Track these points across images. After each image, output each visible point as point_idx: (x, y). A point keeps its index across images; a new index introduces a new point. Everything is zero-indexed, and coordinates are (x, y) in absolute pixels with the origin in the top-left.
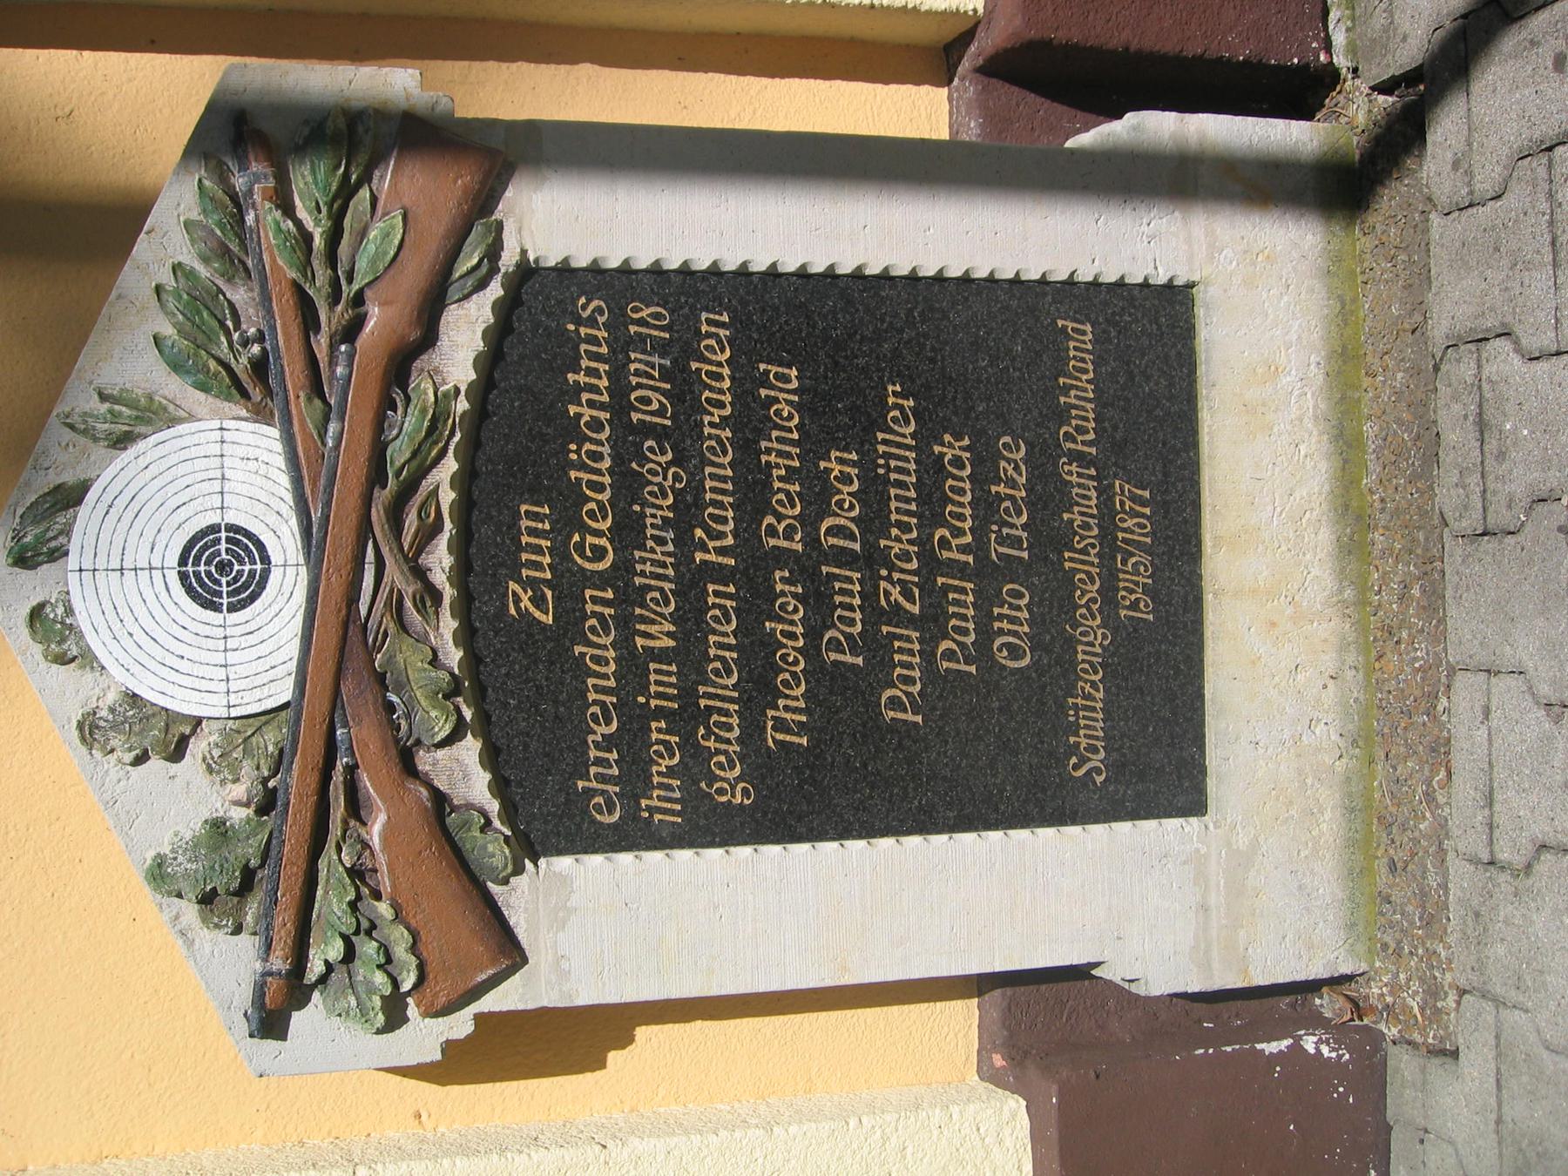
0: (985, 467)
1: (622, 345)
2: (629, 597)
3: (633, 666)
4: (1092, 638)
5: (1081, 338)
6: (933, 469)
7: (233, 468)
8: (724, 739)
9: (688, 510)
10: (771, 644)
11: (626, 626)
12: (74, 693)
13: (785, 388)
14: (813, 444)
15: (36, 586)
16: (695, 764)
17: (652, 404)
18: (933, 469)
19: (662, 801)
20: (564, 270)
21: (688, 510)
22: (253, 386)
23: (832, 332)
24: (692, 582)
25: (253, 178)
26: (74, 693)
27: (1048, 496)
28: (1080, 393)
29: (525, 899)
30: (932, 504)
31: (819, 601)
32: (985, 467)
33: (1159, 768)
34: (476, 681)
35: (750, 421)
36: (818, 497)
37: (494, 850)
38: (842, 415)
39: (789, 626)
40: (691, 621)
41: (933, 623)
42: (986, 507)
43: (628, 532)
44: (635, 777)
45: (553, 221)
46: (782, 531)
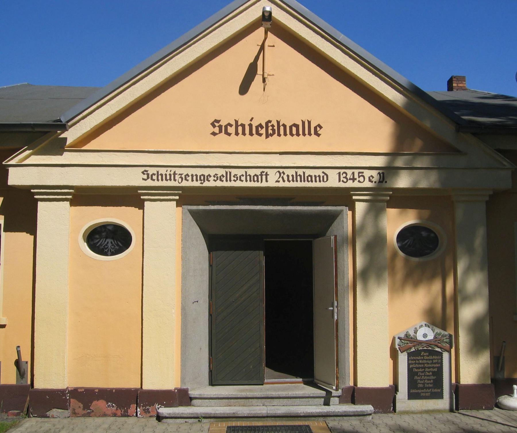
0: (430, 384)
1: (438, 359)
2: (423, 360)
3: (418, 360)
4: (420, 391)
5: (439, 390)
6: (430, 380)
7: (431, 336)
8: (414, 366)
9: (428, 364)
10: (275, 130)
11: (421, 360)
12: (418, 327)
13: (436, 370)
14: (432, 372)
15: (424, 325)
16: (412, 364)
17: (434, 361)
18: (430, 380)
19: (410, 362)
20: (442, 356)
21: (428, 364)
22: (435, 337)
23: (439, 373)
24: (424, 364)
25: (447, 337)
26: (418, 327)
27: (429, 388)
28: (436, 390)
29: (405, 353)
30: (428, 380)
31: (422, 372)
32: (430, 384)
33: (412, 396)
34: (418, 350)
35: (433, 368)
36: (429, 372)
37: (408, 351)
38: (434, 373)
39: (421, 370)
40: (421, 364)
41: (421, 380)
42: (428, 384)
43: (427, 360)
44: (412, 360)
45: (446, 355)
46: (427, 370)
